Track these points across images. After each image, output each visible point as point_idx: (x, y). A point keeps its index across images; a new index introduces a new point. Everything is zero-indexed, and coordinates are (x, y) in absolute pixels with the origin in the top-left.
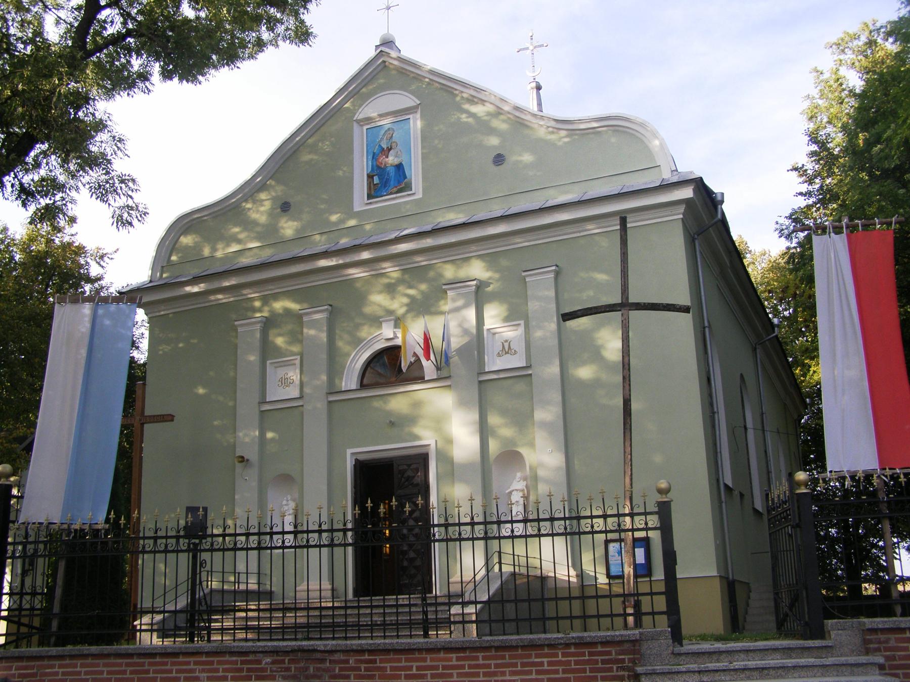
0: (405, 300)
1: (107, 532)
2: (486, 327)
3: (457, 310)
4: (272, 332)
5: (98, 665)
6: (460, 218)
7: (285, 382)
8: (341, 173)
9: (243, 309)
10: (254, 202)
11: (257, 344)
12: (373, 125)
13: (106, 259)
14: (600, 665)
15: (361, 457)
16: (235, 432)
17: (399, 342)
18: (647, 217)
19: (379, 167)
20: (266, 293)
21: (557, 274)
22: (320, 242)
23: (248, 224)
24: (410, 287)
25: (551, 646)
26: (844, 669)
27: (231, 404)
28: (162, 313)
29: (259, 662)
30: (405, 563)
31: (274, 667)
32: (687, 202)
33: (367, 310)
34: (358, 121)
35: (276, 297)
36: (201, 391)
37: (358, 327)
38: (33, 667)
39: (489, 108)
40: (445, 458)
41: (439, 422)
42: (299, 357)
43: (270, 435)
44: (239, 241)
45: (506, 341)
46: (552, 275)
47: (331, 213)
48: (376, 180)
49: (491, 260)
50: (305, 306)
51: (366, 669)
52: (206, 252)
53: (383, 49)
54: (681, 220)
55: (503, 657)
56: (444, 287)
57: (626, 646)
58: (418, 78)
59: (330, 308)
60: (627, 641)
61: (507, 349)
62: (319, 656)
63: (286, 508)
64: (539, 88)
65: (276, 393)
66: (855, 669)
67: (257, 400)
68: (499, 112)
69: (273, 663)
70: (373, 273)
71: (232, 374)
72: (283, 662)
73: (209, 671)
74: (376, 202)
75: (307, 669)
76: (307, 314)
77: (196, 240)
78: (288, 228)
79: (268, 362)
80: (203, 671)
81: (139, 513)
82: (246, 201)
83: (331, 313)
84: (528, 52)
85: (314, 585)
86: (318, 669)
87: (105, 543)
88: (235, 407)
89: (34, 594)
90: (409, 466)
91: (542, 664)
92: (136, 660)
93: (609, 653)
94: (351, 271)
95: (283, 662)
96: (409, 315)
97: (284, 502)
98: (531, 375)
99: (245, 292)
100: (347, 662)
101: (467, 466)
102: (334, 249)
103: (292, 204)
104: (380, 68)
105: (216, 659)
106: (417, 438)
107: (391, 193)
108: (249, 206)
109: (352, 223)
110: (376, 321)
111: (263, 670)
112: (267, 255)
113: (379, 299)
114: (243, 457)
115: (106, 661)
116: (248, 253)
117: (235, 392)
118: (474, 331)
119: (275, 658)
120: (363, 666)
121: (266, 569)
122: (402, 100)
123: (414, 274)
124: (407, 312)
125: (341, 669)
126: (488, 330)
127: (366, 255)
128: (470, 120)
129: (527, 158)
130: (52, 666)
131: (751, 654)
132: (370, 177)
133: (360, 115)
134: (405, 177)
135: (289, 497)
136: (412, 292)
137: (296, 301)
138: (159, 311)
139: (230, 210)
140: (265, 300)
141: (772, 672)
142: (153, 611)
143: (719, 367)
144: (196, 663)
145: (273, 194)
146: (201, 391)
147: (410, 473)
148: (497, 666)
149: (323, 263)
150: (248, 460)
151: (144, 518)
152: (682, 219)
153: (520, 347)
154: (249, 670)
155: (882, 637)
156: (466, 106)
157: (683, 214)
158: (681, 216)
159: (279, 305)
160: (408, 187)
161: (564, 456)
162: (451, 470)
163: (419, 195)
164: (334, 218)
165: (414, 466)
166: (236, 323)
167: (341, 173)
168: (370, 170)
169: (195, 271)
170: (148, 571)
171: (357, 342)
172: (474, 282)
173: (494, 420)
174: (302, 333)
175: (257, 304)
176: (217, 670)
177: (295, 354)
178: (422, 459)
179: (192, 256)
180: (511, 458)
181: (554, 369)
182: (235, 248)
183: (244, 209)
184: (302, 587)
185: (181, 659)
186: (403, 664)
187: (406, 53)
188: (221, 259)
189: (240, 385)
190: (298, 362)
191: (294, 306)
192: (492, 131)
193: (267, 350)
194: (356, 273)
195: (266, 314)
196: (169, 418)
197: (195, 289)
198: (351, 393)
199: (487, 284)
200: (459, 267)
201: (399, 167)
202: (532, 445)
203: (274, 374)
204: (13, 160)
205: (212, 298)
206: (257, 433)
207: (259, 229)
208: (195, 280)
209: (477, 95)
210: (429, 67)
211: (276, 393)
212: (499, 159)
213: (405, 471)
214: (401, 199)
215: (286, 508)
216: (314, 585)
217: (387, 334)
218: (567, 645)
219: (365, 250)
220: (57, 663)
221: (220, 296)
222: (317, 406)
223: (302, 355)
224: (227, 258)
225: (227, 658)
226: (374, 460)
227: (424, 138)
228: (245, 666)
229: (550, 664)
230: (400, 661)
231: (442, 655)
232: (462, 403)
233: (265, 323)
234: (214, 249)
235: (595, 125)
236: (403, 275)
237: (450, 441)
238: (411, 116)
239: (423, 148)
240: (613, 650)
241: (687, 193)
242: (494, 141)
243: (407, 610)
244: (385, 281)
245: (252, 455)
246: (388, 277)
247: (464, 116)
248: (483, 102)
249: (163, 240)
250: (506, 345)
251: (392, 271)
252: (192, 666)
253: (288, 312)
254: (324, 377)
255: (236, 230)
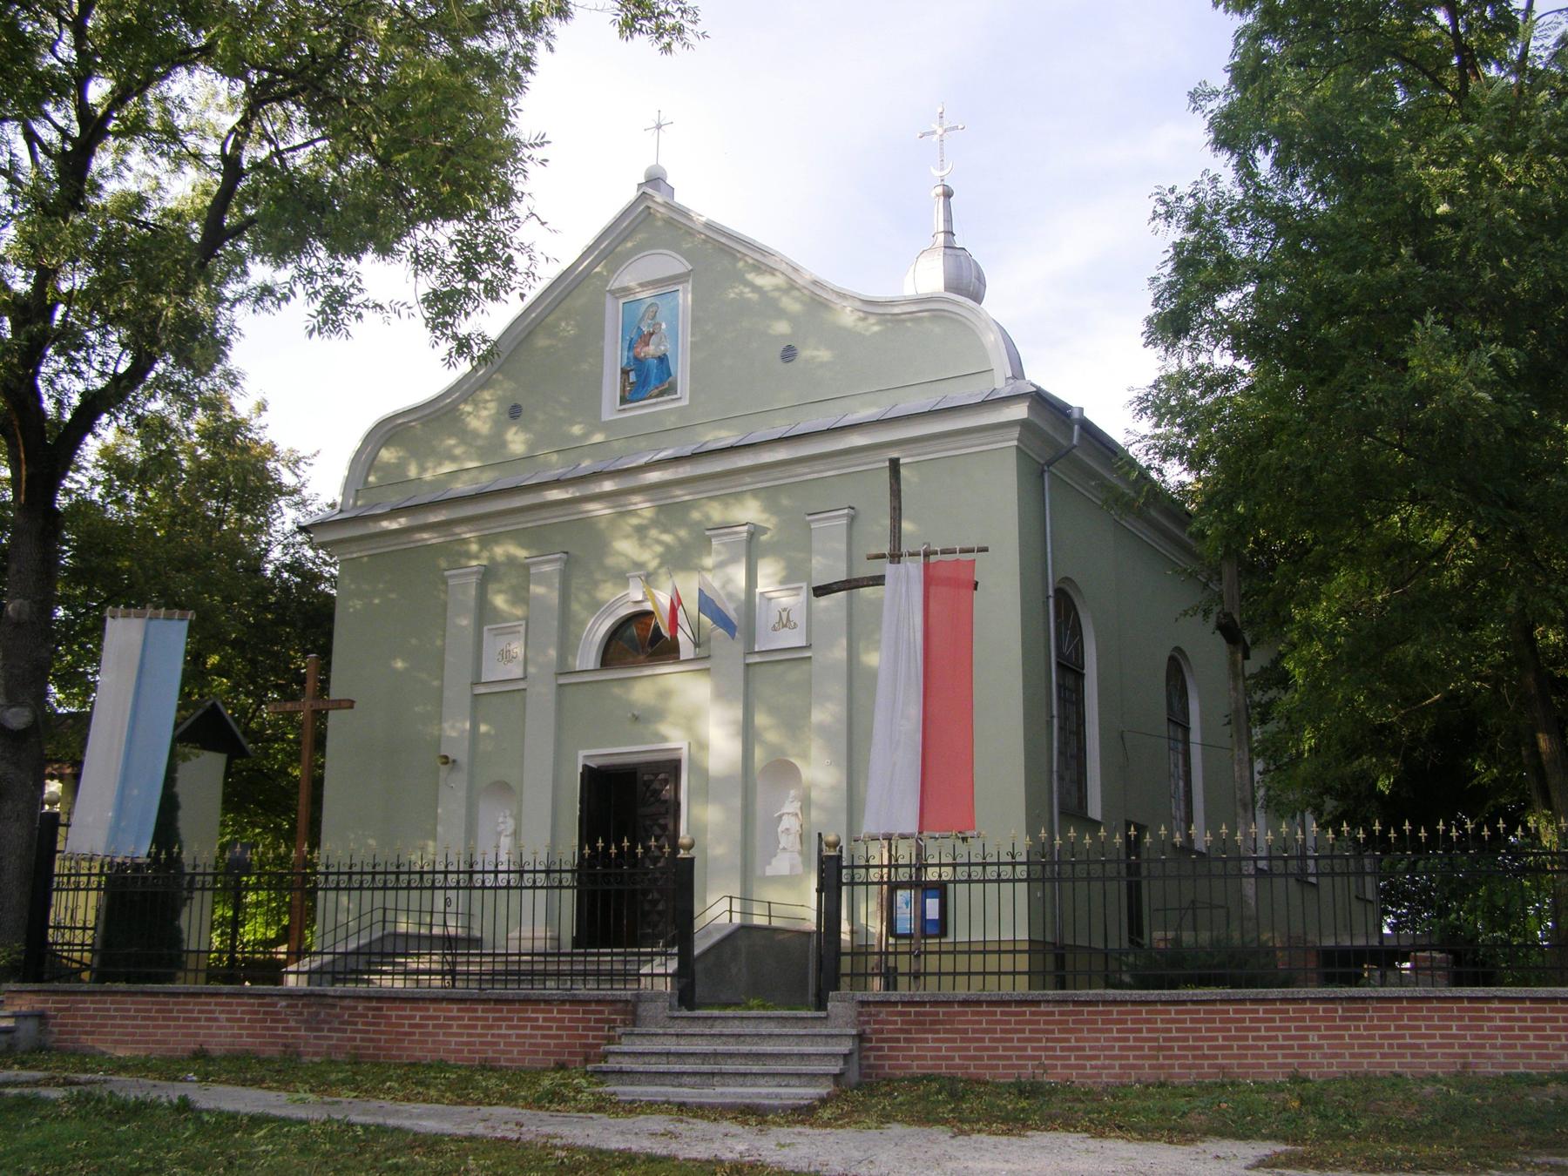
0: (659, 549)
1: (149, 866)
2: (759, 590)
3: (721, 565)
4: (492, 587)
5: (105, 1002)
6: (727, 437)
7: (506, 656)
8: (585, 367)
9: (455, 552)
10: (476, 404)
11: (472, 603)
12: (631, 298)
13: (302, 465)
14: (592, 1024)
15: (592, 764)
16: (440, 723)
17: (648, 606)
18: (969, 443)
19: (636, 359)
20: (487, 532)
21: (852, 520)
22: (556, 466)
23: (466, 436)
24: (666, 531)
25: (547, 1002)
26: (819, 1039)
27: (436, 683)
28: (355, 555)
29: (274, 1005)
30: (647, 907)
31: (289, 1011)
32: (1023, 424)
33: (610, 561)
34: (612, 292)
35: (495, 538)
36: (399, 664)
37: (596, 584)
38: (67, 1002)
39: (779, 280)
40: (700, 771)
41: (690, 721)
42: (523, 623)
43: (483, 728)
44: (454, 459)
45: (785, 610)
46: (844, 521)
47: (573, 423)
48: (632, 377)
49: (769, 496)
50: (535, 553)
51: (374, 1017)
52: (413, 472)
53: (645, 189)
54: (1014, 450)
55: (501, 1011)
56: (708, 533)
57: (620, 1006)
58: (690, 232)
59: (564, 556)
60: (620, 1001)
61: (785, 622)
62: (330, 1001)
63: (502, 826)
64: (948, 194)
65: (494, 671)
66: (829, 1040)
67: (469, 681)
68: (792, 286)
69: (288, 1006)
70: (619, 509)
71: (439, 642)
72: (296, 1006)
73: (229, 1012)
74: (630, 409)
75: (318, 1014)
76: (534, 564)
77: (401, 454)
78: (516, 441)
79: (485, 628)
80: (222, 1012)
81: (180, 848)
82: (465, 401)
83: (567, 563)
84: (935, 138)
85: (527, 933)
86: (329, 1014)
87: (145, 879)
88: (441, 690)
89: (84, 928)
90: (657, 775)
91: (537, 1019)
92: (162, 999)
93: (601, 1012)
94: (591, 506)
95: (296, 1006)
96: (663, 570)
97: (501, 820)
98: (810, 658)
99: (457, 530)
100: (355, 1008)
101: (725, 780)
102: (569, 476)
103: (524, 407)
104: (643, 216)
105: (235, 1001)
106: (664, 739)
107: (651, 397)
108: (468, 408)
109: (598, 438)
110: (622, 578)
111: (278, 1013)
112: (487, 480)
113: (626, 547)
114: (446, 757)
115: (135, 999)
116: (465, 477)
117: (442, 668)
118: (743, 596)
119: (290, 1002)
120: (370, 1013)
121: (476, 910)
122: (668, 263)
123: (670, 514)
124: (661, 565)
125: (350, 1016)
126: (762, 594)
127: (608, 486)
128: (754, 296)
129: (824, 355)
130: (85, 1002)
131: (745, 1022)
132: (625, 372)
133: (615, 284)
134: (670, 375)
135: (508, 813)
136: (667, 538)
137: (523, 546)
138: (352, 553)
139: (445, 414)
140: (485, 542)
141: (748, 1039)
142: (322, 953)
143: (1094, 646)
144: (217, 1004)
145: (500, 393)
146: (399, 664)
147: (656, 785)
148: (495, 1019)
149: (555, 495)
150: (454, 761)
151: (184, 855)
152: (1017, 447)
153: (799, 617)
154: (266, 1013)
155: (873, 1009)
156: (751, 277)
157: (1018, 440)
158: (1015, 443)
159: (500, 551)
160: (672, 389)
161: (845, 771)
162: (707, 787)
163: (685, 402)
164: (577, 430)
165: (661, 776)
166: (447, 573)
167: (585, 367)
168: (625, 361)
169: (396, 500)
170: (331, 905)
171: (595, 606)
172: (746, 528)
173: (761, 719)
174: (528, 590)
175: (474, 547)
176: (235, 1012)
177: (519, 619)
178: (672, 768)
179: (395, 478)
180: (783, 770)
181: (839, 653)
182: (448, 467)
183: (462, 414)
184: (514, 934)
185: (203, 1000)
186: (408, 1013)
187: (680, 199)
188: (430, 483)
189: (449, 658)
190: (522, 629)
191: (521, 553)
192: (781, 313)
193: (484, 613)
194: (598, 509)
195: (485, 562)
196: (350, 704)
197: (394, 525)
198: (585, 675)
199: (764, 530)
200: (727, 506)
201: (662, 359)
202: (805, 756)
203: (491, 645)
204: (126, 387)
205: (418, 536)
206: (468, 725)
207: (480, 442)
208: (394, 513)
209: (762, 259)
210: (704, 219)
211: (494, 671)
212: (789, 354)
213: (652, 781)
214: (663, 406)
215: (502, 826)
216: (527, 933)
217: (634, 596)
218: (563, 1002)
219: (607, 479)
220: (90, 998)
221: (425, 536)
222: (542, 694)
223: (527, 619)
224: (438, 483)
225: (246, 1000)
226: (613, 766)
227: (696, 321)
228: (262, 1009)
229: (545, 1019)
230: (404, 1009)
231: (444, 1005)
232: (720, 695)
233: (484, 575)
234: (423, 469)
235: (914, 308)
236: (657, 514)
237: (703, 746)
238: (680, 287)
239: (693, 335)
240: (606, 1009)
241: (1020, 411)
242: (782, 327)
243: (478, 959)
244: (635, 521)
245: (460, 753)
246: (639, 516)
247: (747, 290)
248: (772, 271)
249: (359, 453)
250: (784, 615)
251: (643, 507)
252: (213, 1007)
253: (511, 561)
254: (553, 653)
255: (452, 442)
